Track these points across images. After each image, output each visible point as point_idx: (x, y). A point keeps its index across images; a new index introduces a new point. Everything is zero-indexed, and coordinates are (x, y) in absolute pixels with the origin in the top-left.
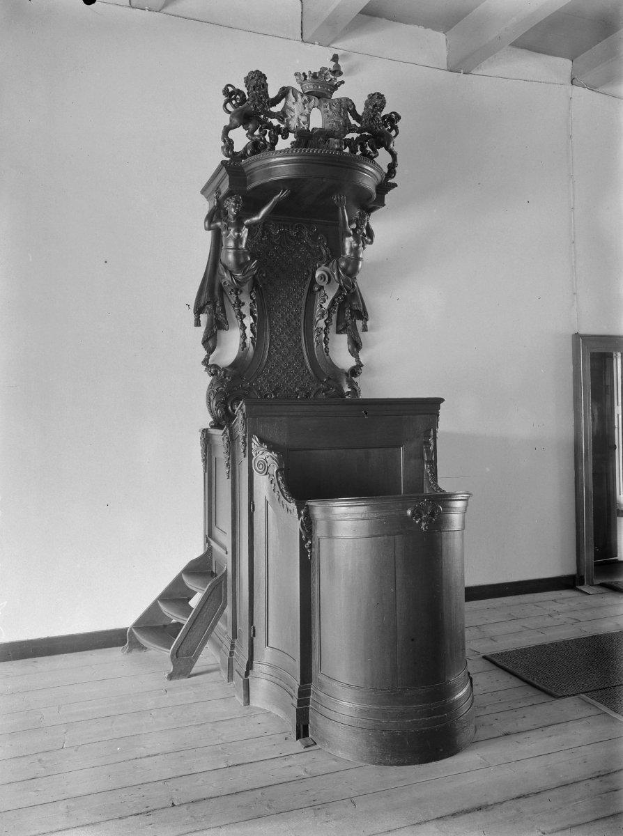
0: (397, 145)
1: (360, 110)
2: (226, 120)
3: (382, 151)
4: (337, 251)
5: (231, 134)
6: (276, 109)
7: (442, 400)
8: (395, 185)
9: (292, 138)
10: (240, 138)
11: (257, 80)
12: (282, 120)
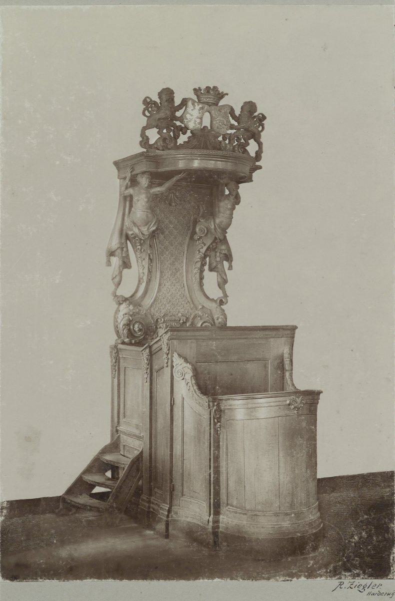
0: (264, 137)
1: (237, 112)
2: (144, 121)
3: (252, 142)
4: (369, 577)
5: (148, 133)
6: (178, 114)
7: (322, 392)
8: (260, 167)
9: (189, 134)
10: (153, 135)
11: (167, 94)
12: (182, 122)
